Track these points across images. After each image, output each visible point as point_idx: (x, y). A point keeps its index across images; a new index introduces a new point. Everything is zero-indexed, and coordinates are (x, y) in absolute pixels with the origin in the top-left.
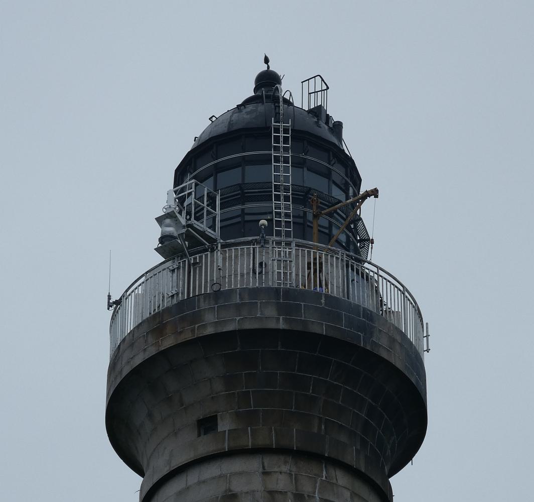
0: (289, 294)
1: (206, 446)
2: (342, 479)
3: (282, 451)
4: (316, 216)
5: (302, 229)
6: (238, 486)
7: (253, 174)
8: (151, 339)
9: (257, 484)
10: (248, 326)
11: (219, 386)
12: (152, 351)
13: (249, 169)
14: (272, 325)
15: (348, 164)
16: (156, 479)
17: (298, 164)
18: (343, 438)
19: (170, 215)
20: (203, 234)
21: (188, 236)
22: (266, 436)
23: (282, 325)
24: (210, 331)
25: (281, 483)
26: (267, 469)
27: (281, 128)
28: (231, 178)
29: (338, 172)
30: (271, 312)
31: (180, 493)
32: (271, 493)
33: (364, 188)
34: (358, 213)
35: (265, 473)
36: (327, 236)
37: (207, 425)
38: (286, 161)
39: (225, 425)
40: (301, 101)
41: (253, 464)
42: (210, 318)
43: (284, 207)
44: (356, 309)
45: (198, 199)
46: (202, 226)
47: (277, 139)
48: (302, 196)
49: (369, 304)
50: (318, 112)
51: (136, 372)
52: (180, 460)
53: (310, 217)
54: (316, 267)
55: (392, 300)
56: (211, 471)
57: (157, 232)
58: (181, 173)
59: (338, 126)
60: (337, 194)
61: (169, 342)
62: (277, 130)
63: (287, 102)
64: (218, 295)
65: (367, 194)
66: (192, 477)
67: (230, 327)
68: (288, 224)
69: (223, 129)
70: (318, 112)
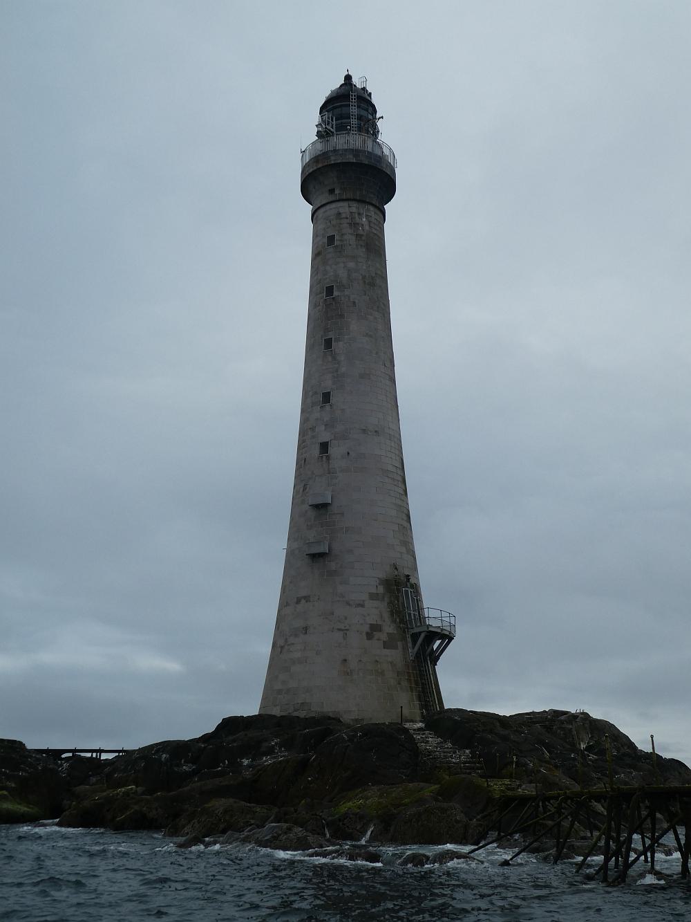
0: (357, 151)
1: (332, 198)
2: (372, 208)
3: (354, 200)
4: (364, 125)
5: (360, 129)
6: (341, 210)
7: (345, 109)
8: (315, 164)
9: (347, 210)
10: (344, 161)
11: (335, 179)
12: (315, 168)
13: (344, 108)
14: (352, 161)
15: (373, 106)
16: (317, 207)
17: (359, 107)
18: (372, 196)
19: (320, 124)
20: (329, 130)
21: (325, 131)
22: (350, 195)
23: (354, 161)
24: (333, 162)
25: (354, 210)
26: (332, 451)
27: (353, 96)
28: (338, 111)
29: (370, 110)
30: (351, 156)
31: (324, 212)
32: (351, 213)
33: (378, 116)
34: (110, 756)
35: (349, 207)
36: (368, 132)
37: (332, 191)
38: (355, 106)
39: (337, 192)
40: (359, 86)
41: (346, 204)
42: (333, 158)
43: (354, 121)
44: (376, 155)
45: (613, 882)
46: (329, 127)
47: (352, 99)
48: (360, 118)
49: (379, 153)
50: (364, 89)
51: (310, 174)
52: (324, 202)
53: (362, 125)
54: (364, 141)
55: (386, 152)
56: (333, 205)
57: (316, 129)
58: (322, 109)
59: (370, 93)
60: (370, 117)
61: (320, 166)
62: (352, 96)
63: (355, 86)
64: (335, 151)
65: (380, 118)
66: (328, 207)
67: (339, 162)
68: (356, 127)
69: (335, 95)
70: (364, 89)
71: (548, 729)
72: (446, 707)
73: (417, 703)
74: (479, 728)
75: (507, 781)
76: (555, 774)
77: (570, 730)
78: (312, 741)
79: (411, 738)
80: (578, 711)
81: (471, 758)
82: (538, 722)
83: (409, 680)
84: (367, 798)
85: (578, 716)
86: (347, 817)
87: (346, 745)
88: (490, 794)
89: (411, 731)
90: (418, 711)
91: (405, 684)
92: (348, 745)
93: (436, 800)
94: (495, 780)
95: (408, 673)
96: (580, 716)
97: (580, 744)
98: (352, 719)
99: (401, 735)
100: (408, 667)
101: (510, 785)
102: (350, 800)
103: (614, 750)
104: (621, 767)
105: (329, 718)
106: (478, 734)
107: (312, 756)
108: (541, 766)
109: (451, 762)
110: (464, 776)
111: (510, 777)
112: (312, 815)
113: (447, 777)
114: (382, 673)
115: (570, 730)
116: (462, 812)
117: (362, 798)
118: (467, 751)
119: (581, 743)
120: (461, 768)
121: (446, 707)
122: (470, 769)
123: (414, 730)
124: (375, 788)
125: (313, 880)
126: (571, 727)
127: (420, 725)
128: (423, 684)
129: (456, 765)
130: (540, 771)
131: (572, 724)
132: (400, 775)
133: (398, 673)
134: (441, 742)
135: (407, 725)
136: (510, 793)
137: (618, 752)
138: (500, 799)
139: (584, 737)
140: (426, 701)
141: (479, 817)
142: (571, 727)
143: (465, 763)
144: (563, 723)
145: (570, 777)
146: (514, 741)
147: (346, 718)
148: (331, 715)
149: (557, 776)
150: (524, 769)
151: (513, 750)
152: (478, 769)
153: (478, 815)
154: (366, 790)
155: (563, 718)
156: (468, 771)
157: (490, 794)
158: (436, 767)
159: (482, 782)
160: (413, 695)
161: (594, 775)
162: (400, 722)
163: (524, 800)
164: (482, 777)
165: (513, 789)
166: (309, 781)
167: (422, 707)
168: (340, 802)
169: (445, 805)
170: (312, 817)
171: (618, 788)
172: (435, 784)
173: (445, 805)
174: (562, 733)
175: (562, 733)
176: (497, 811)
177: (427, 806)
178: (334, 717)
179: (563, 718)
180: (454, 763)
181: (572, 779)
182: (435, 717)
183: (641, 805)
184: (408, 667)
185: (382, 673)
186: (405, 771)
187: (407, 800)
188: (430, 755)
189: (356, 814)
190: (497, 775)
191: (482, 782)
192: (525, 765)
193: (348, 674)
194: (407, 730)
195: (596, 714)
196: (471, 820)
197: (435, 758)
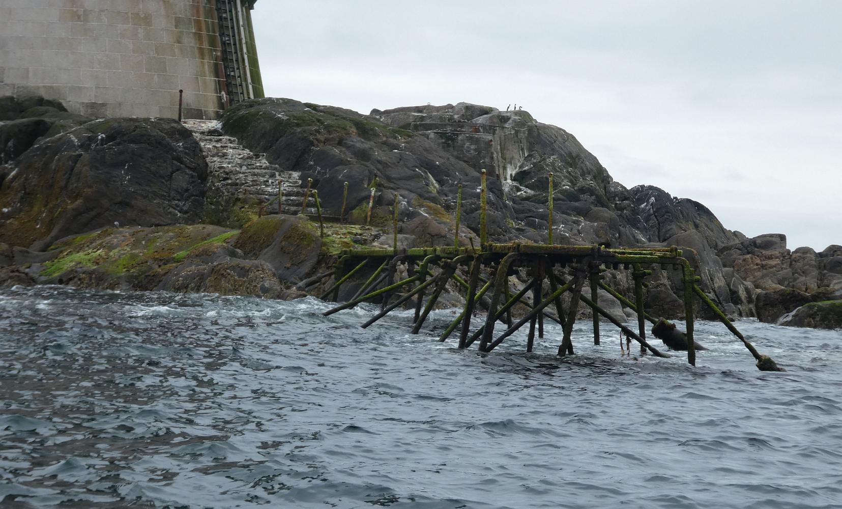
71: (448, 140)
72: (267, 95)
73: (211, 79)
74: (319, 136)
75: (356, 229)
76: (445, 220)
77: (489, 144)
78: (10, 144)
79: (195, 149)
80: (512, 109)
81: (301, 186)
82: (428, 127)
83: (198, 36)
84: (111, 247)
85: (508, 119)
86: (74, 277)
87: (77, 153)
88: (324, 248)
89: (197, 136)
90: (212, 95)
91: (189, 42)
92: (80, 155)
93: (233, 254)
94: (335, 225)
95: (198, 22)
96: (513, 117)
97: (505, 168)
98: (83, 103)
99: (178, 141)
100: (198, 11)
101: (361, 235)
102: (80, 249)
103: (565, 182)
104: (563, 213)
105: (41, 101)
106: (318, 146)
107: (12, 169)
108: (421, 206)
109: (263, 193)
110: (283, 217)
111: (363, 222)
112: (13, 272)
113: (255, 218)
114: (146, 20)
115: (489, 144)
116: (274, 275)
117: (101, 246)
118: (296, 175)
119: (509, 166)
120: (280, 204)
121: (267, 95)
122: (297, 205)
123: (203, 133)
124: (127, 231)
125: (149, 235)
126: (490, 137)
127: (215, 124)
128: (224, 43)
129: (272, 198)
130: (419, 213)
131: (494, 133)
132: (171, 210)
133: (178, 22)
134: (250, 158)
135: (190, 124)
136: (359, 248)
137: (573, 184)
138: (340, 257)
139: (516, 156)
140: (228, 76)
141: (301, 284)
142: (490, 137)
143: (289, 194)
144: (477, 131)
145: (468, 227)
146: (379, 162)
147: (73, 102)
148: (46, 97)
149: (445, 223)
150: (391, 209)
151: (376, 176)
152: (309, 205)
153: (301, 280)
154: (109, 235)
155: (480, 120)
156: (293, 208)
157: (324, 248)
158: (238, 199)
159: (313, 228)
160: (203, 63)
161: (513, 224)
162: (176, 117)
163: (376, 260)
164: (313, 218)
165: (364, 242)
166: (3, 213)
167: (219, 87)
168: (61, 252)
169: (247, 263)
170: (11, 274)
171: (491, 245)
172: (233, 228)
173: (247, 263)
174: (473, 147)
175: (473, 147)
176: (333, 277)
177: (215, 264)
178: (50, 99)
179: (480, 120)
180: (270, 194)
181: (472, 229)
182: (242, 112)
183: (482, 266)
184: (198, 11)
185: (146, 20)
186: (181, 204)
187: (182, 254)
188: (228, 179)
189: (90, 273)
190: (343, 218)
191: (313, 228)
192: (391, 203)
193: (79, 17)
194: (187, 134)
195: (542, 116)
196: (288, 288)
197: (237, 184)
